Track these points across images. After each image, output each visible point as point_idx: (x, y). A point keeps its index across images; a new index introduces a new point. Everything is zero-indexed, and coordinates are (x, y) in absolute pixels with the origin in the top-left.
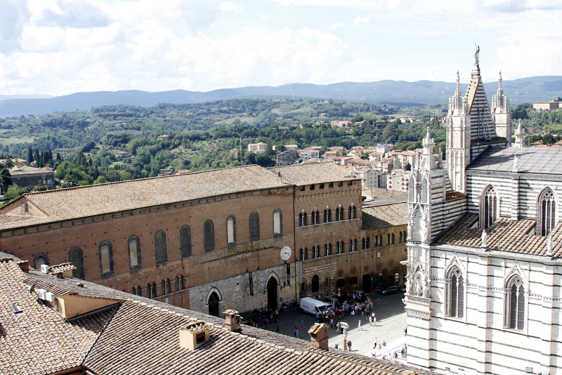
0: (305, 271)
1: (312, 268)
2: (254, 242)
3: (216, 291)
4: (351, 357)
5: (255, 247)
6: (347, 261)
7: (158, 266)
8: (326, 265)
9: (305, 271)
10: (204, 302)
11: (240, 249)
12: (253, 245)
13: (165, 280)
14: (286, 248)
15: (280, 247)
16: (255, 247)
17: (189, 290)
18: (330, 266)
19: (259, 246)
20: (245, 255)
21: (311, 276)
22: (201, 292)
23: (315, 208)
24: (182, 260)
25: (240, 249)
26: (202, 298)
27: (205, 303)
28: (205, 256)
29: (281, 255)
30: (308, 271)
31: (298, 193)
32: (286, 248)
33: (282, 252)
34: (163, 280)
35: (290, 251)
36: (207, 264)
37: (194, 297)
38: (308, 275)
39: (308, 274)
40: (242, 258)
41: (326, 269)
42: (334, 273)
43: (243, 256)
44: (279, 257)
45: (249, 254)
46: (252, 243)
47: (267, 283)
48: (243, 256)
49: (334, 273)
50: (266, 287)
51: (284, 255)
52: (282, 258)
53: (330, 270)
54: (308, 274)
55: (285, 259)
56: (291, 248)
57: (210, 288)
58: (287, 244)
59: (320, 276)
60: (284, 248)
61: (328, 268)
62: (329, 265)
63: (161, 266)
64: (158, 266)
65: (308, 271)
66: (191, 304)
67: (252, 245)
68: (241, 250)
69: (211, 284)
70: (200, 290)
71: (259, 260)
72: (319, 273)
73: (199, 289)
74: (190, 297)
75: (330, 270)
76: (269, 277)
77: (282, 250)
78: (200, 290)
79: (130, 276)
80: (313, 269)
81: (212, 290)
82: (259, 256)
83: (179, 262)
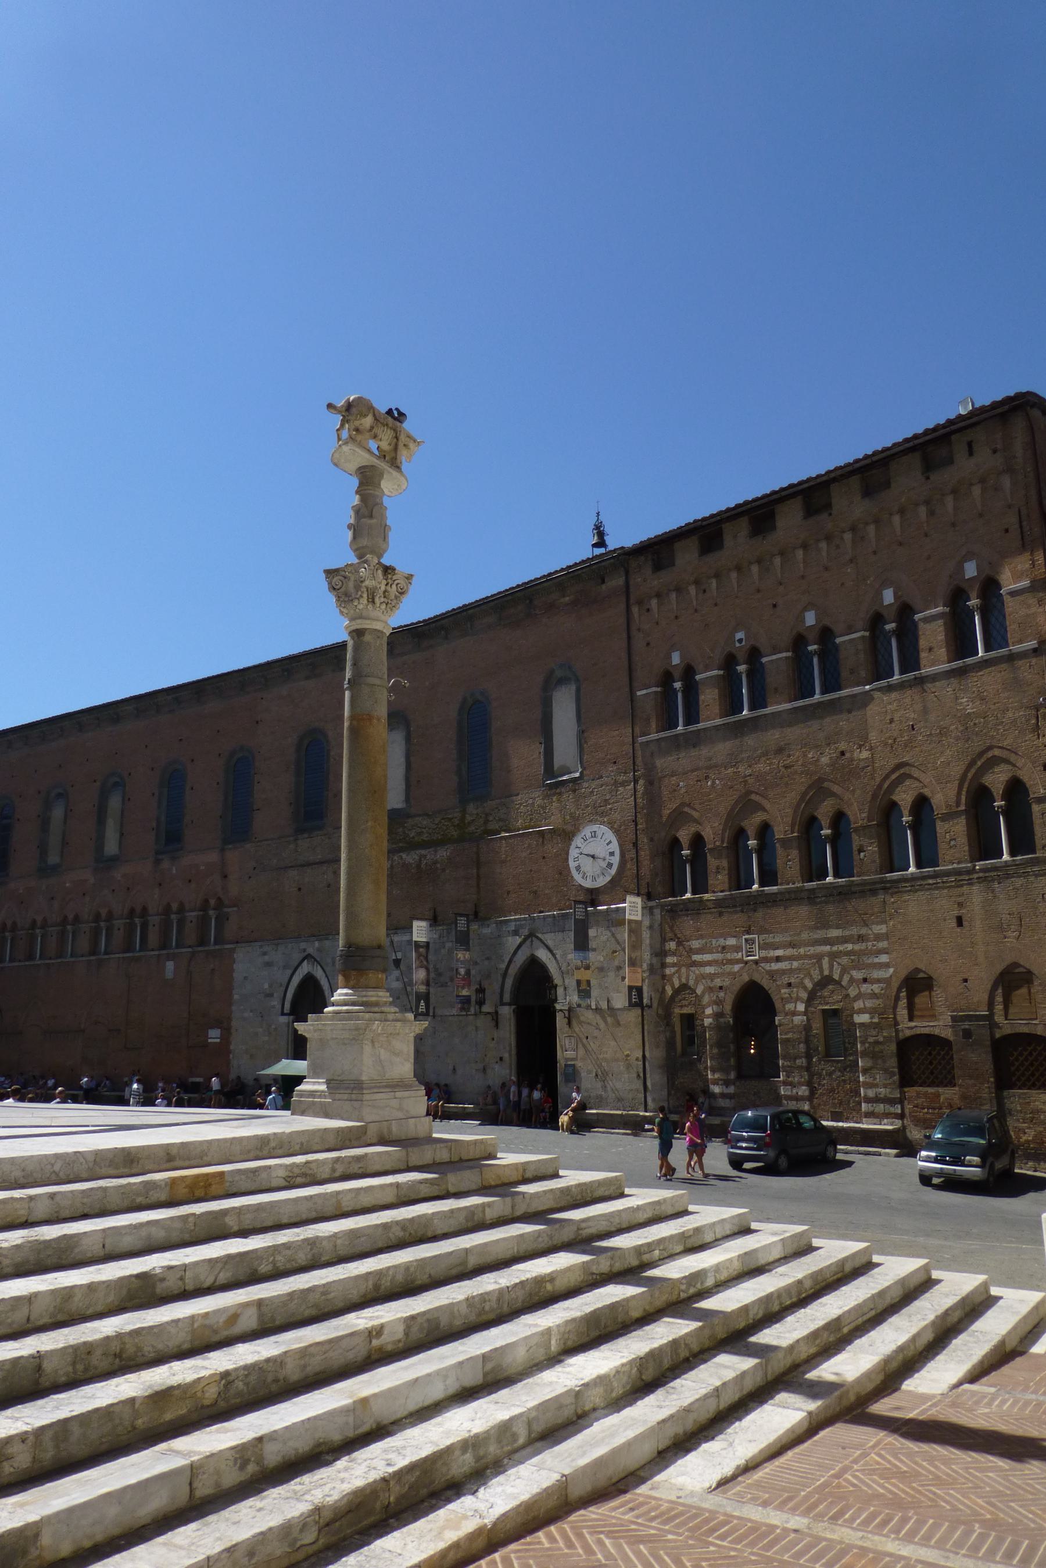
0: (691, 951)
1: (732, 942)
2: (471, 808)
3: (319, 974)
4: (566, 1455)
5: (472, 828)
6: (960, 921)
7: (157, 862)
8: (820, 934)
9: (691, 951)
10: (276, 1003)
11: (420, 834)
12: (468, 818)
13: (175, 906)
14: (594, 835)
15: (569, 828)
16: (472, 828)
17: (233, 950)
18: (845, 940)
19: (486, 822)
20: (429, 854)
21: (727, 982)
22: (268, 964)
23: (740, 635)
24: (223, 850)
25: (420, 834)
26: (271, 986)
27: (279, 1007)
28: (292, 846)
29: (572, 864)
30: (707, 957)
31: (646, 580)
32: (594, 835)
33: (573, 853)
34: (169, 905)
35: (615, 847)
36: (293, 873)
37: (246, 978)
38: (712, 977)
39: (709, 970)
40: (418, 866)
41: (819, 958)
42: (876, 988)
43: (422, 857)
44: (563, 873)
45: (443, 853)
46: (464, 812)
47: (509, 982)
48: (422, 857)
49: (876, 988)
50: (507, 997)
51: (587, 865)
52: (578, 877)
53: (844, 971)
54: (709, 970)
55: (588, 884)
56: (617, 832)
57: (297, 957)
58: (599, 814)
59: (779, 993)
60: (587, 831)
61: (833, 956)
62: (834, 933)
63: (166, 864)
64: (157, 862)
65: (707, 957)
66: (236, 997)
67: (463, 818)
68: (425, 837)
69: (303, 945)
70: (266, 958)
71: (478, 876)
72: (772, 974)
73: (265, 954)
74: (235, 975)
75: (844, 971)
76: (521, 958)
77: (578, 841)
78: (266, 958)
79: (92, 881)
80: (737, 949)
81: (305, 968)
82: (478, 864)
83: (213, 857)
